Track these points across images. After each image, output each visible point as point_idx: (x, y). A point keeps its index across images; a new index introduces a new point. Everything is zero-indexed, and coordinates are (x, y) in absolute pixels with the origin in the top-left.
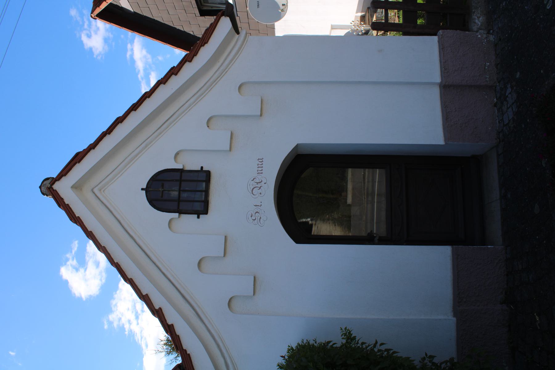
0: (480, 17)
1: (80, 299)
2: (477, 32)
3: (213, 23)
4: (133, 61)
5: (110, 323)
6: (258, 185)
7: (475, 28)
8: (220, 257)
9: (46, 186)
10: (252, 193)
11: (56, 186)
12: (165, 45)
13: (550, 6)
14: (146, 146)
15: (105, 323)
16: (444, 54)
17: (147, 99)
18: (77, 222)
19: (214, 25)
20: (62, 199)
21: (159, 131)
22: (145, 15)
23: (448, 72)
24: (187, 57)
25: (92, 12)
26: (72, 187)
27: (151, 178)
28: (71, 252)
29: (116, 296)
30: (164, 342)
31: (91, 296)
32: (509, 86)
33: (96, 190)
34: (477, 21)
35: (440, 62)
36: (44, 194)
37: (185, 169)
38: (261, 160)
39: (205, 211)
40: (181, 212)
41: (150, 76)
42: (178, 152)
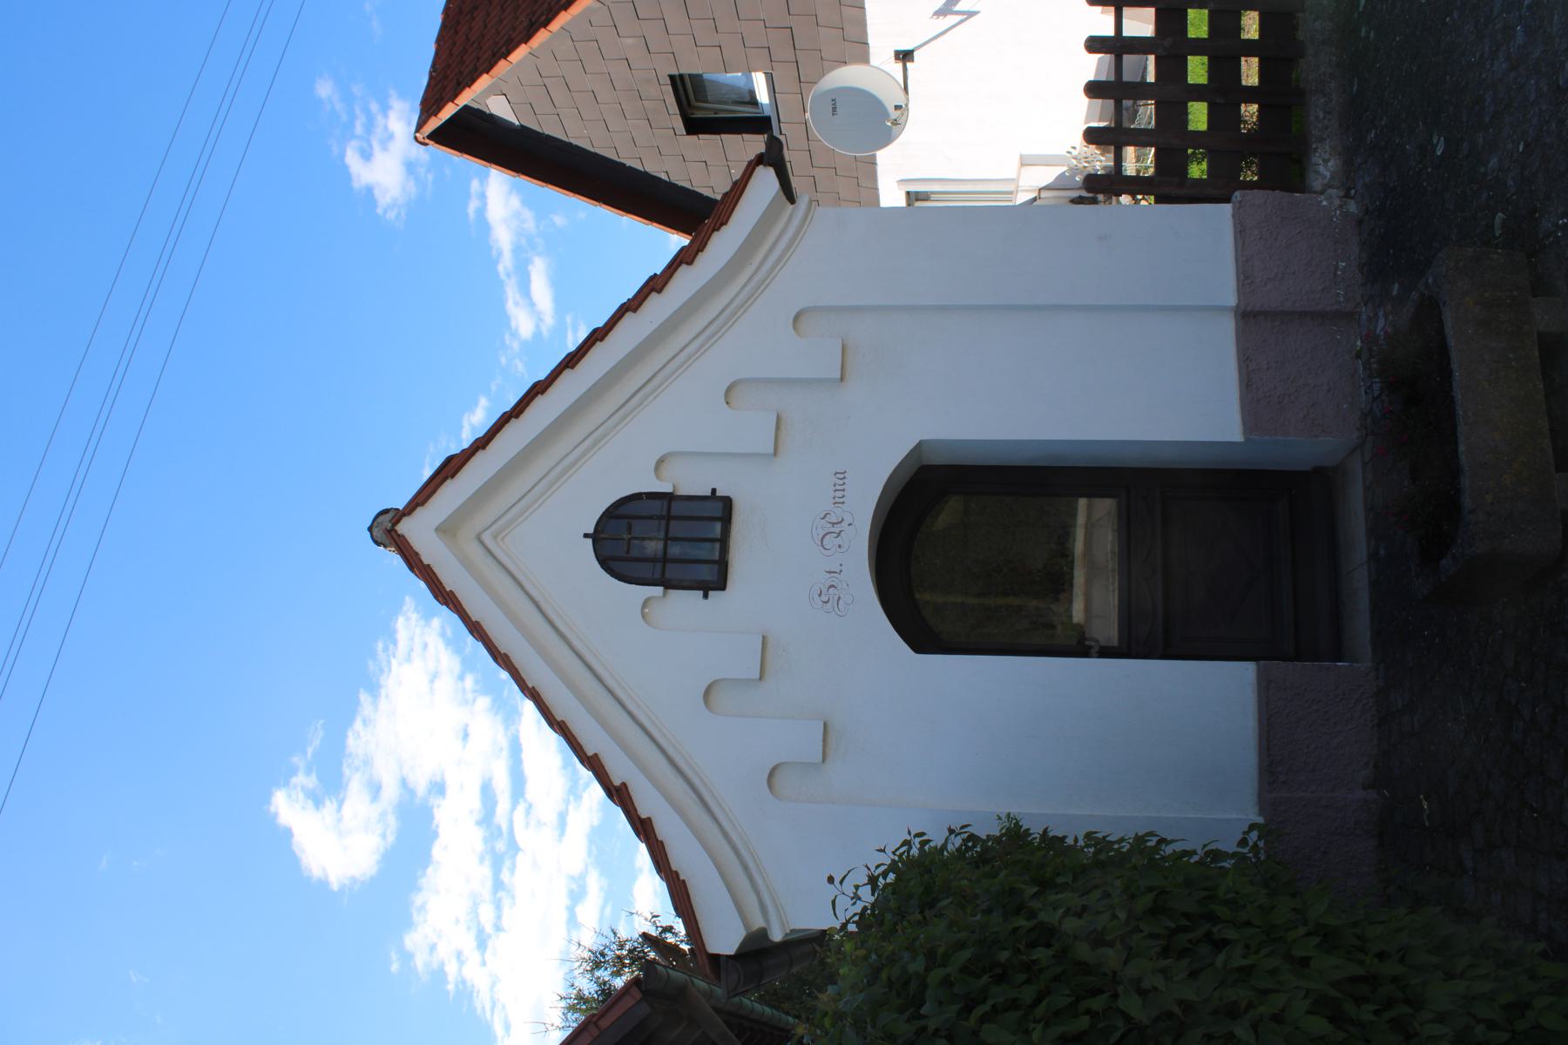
0: (1328, 160)
1: (323, 884)
2: (1322, 193)
3: (740, 179)
4: (484, 226)
5: (407, 957)
6: (834, 528)
7: (1317, 185)
8: (752, 680)
9: (384, 527)
10: (822, 543)
11: (404, 528)
12: (596, 206)
13: (1441, 150)
14: (594, 444)
15: (394, 956)
16: (1244, 243)
17: (598, 343)
18: (450, 601)
19: (742, 186)
20: (417, 554)
21: (622, 412)
22: (546, 133)
23: (1252, 282)
24: (683, 253)
25: (419, 127)
26: (436, 529)
27: (604, 513)
28: (305, 753)
29: (423, 881)
30: (568, 1001)
31: (354, 880)
32: (1381, 313)
33: (487, 537)
34: (1321, 169)
35: (1237, 261)
36: (378, 543)
37: (679, 494)
38: (841, 475)
39: (721, 585)
40: (668, 585)
41: (530, 268)
42: (662, 457)
